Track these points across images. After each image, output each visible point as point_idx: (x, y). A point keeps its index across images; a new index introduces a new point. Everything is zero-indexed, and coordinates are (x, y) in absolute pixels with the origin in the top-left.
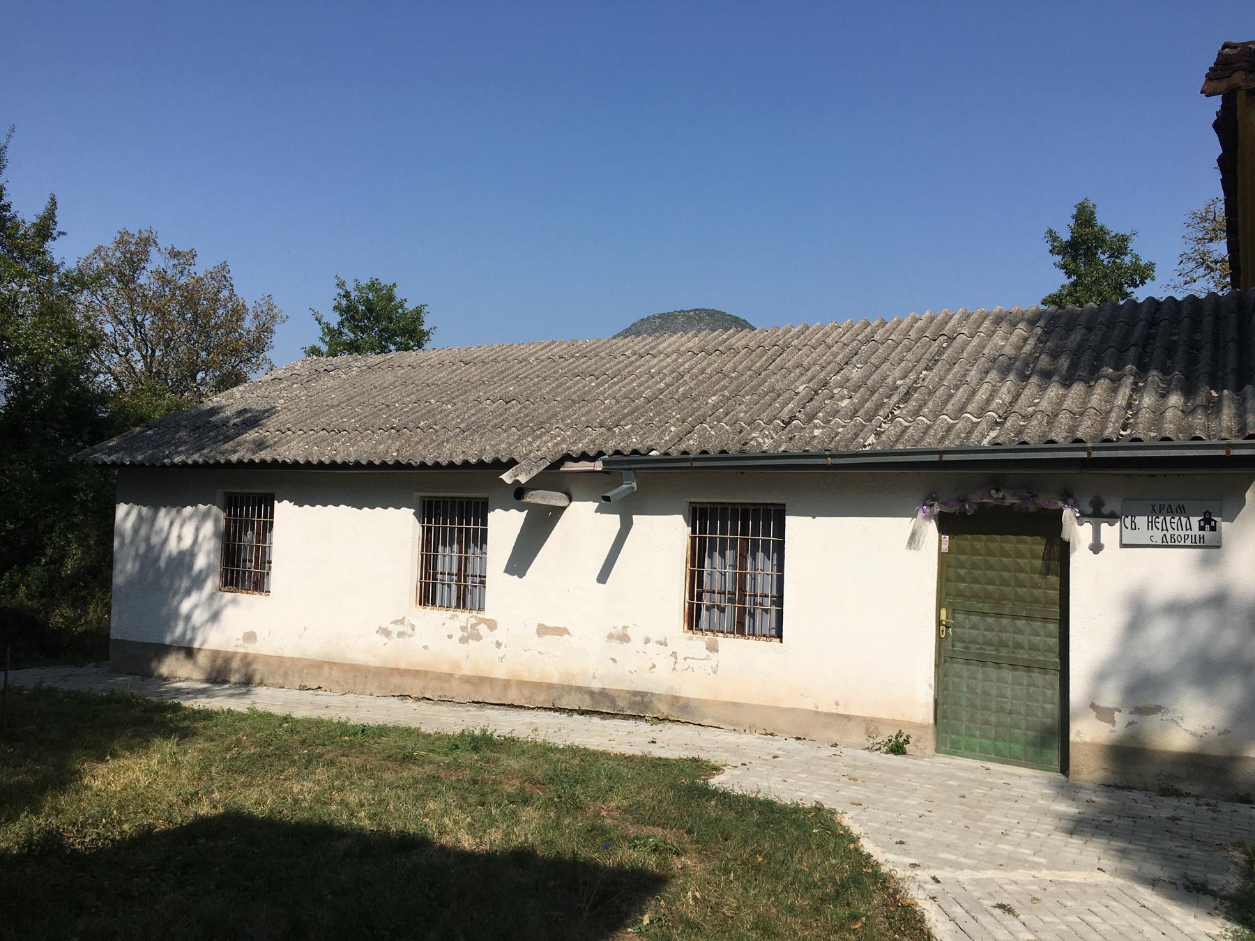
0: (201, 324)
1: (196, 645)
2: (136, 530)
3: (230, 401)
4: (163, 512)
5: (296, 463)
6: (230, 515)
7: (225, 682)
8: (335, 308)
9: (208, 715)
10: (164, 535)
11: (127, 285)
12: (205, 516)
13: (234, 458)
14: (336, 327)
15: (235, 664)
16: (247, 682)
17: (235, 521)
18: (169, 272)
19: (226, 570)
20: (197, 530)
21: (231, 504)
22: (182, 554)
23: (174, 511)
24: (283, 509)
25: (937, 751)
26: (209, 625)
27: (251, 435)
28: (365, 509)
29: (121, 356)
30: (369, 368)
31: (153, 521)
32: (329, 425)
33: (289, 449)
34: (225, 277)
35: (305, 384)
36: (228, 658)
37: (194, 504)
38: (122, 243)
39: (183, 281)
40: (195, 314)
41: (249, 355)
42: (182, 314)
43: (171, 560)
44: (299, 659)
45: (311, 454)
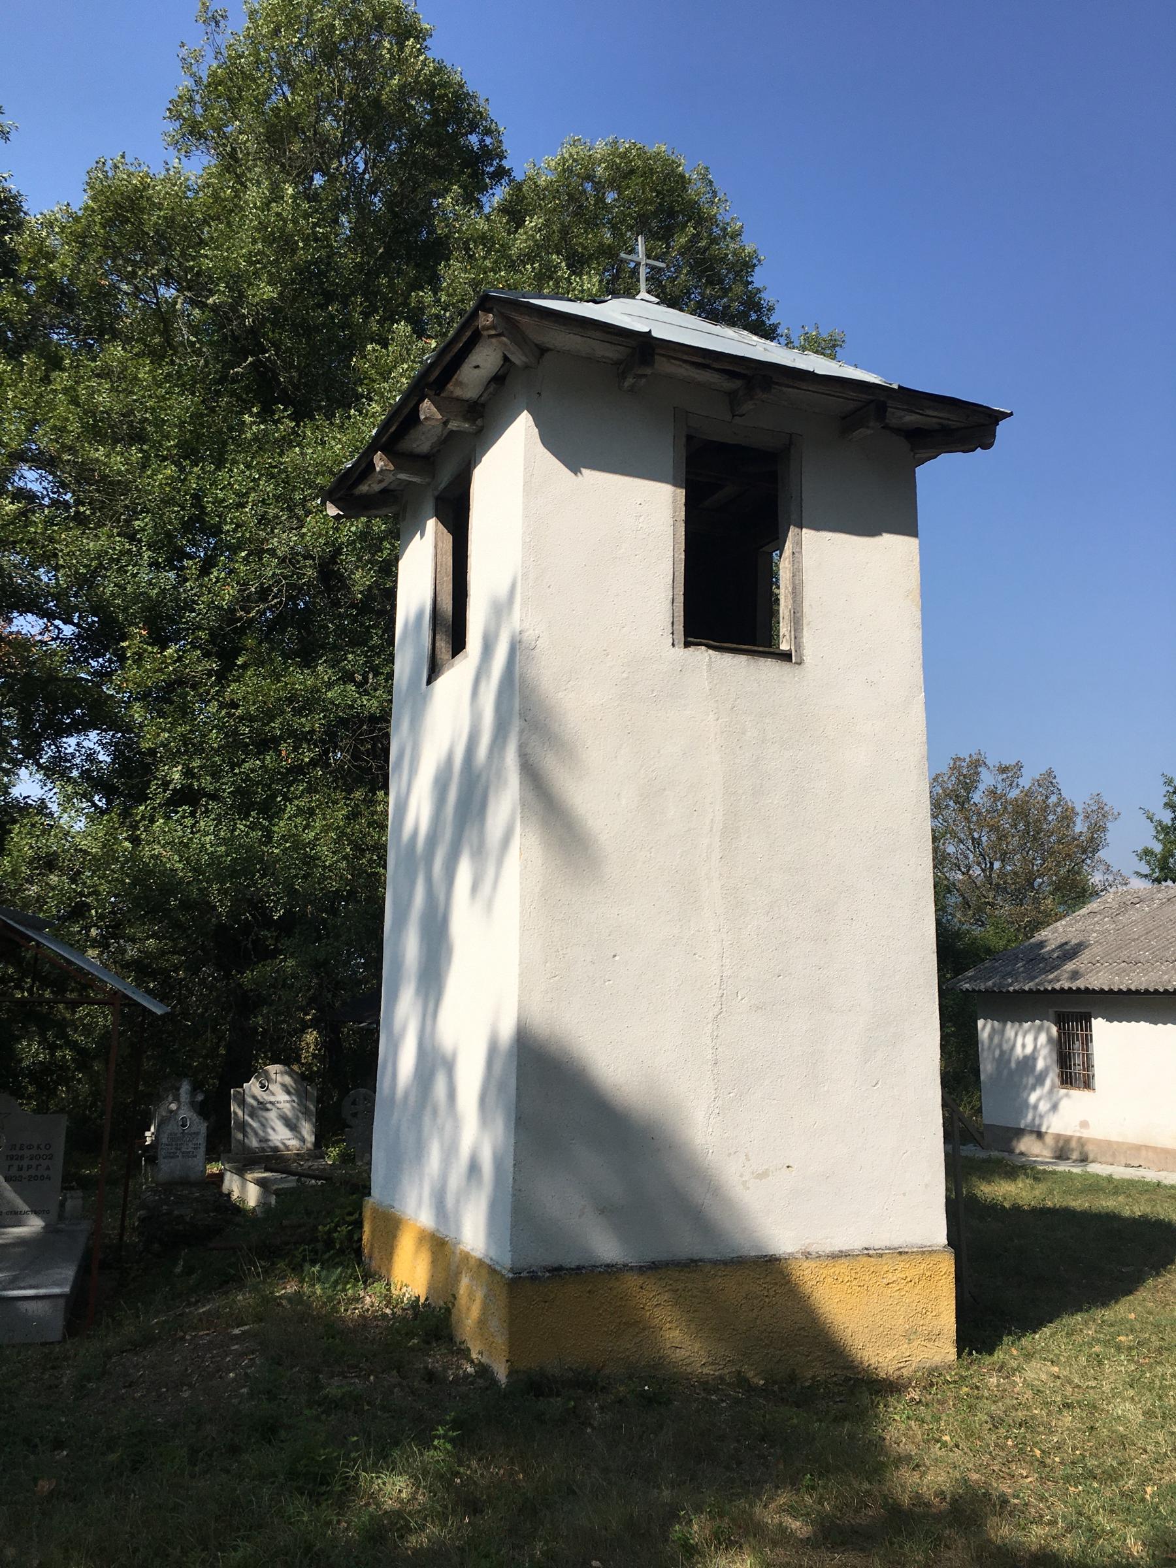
0: (1033, 834)
1: (1043, 1129)
2: (991, 1038)
3: (1053, 935)
4: (1009, 1024)
5: (1102, 990)
6: (1060, 1029)
7: (1068, 1159)
8: (1166, 804)
9: (1054, 1173)
10: (1011, 1043)
11: (963, 804)
12: (1040, 1029)
13: (1057, 986)
14: (1170, 824)
15: (1073, 1144)
16: (1084, 1160)
17: (1064, 1034)
18: (999, 787)
19: (1062, 1072)
20: (1036, 1039)
21: (1061, 1020)
22: (1026, 1058)
23: (1017, 1024)
24: (1099, 1025)
25: (1062, 1083)
26: (1051, 1113)
27: (1070, 966)
28: (1160, 1025)
29: (963, 873)
30: (1168, 900)
31: (1003, 1032)
32: (1128, 957)
33: (1097, 979)
34: (1052, 783)
35: (1114, 918)
36: (1068, 1140)
37: (1033, 1021)
38: (955, 768)
39: (1014, 794)
40: (1027, 824)
41: (1084, 857)
42: (1015, 826)
43: (1018, 1063)
44: (1123, 1143)
45: (1114, 983)
